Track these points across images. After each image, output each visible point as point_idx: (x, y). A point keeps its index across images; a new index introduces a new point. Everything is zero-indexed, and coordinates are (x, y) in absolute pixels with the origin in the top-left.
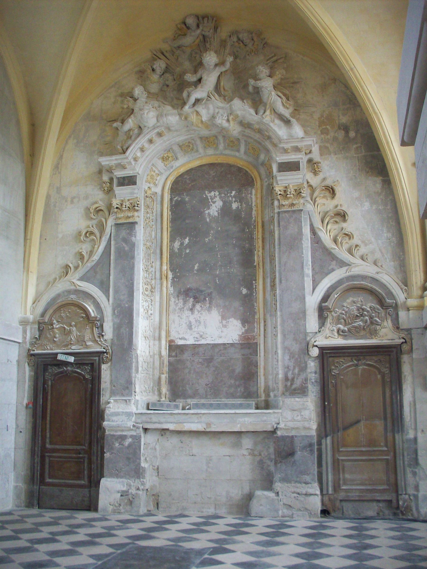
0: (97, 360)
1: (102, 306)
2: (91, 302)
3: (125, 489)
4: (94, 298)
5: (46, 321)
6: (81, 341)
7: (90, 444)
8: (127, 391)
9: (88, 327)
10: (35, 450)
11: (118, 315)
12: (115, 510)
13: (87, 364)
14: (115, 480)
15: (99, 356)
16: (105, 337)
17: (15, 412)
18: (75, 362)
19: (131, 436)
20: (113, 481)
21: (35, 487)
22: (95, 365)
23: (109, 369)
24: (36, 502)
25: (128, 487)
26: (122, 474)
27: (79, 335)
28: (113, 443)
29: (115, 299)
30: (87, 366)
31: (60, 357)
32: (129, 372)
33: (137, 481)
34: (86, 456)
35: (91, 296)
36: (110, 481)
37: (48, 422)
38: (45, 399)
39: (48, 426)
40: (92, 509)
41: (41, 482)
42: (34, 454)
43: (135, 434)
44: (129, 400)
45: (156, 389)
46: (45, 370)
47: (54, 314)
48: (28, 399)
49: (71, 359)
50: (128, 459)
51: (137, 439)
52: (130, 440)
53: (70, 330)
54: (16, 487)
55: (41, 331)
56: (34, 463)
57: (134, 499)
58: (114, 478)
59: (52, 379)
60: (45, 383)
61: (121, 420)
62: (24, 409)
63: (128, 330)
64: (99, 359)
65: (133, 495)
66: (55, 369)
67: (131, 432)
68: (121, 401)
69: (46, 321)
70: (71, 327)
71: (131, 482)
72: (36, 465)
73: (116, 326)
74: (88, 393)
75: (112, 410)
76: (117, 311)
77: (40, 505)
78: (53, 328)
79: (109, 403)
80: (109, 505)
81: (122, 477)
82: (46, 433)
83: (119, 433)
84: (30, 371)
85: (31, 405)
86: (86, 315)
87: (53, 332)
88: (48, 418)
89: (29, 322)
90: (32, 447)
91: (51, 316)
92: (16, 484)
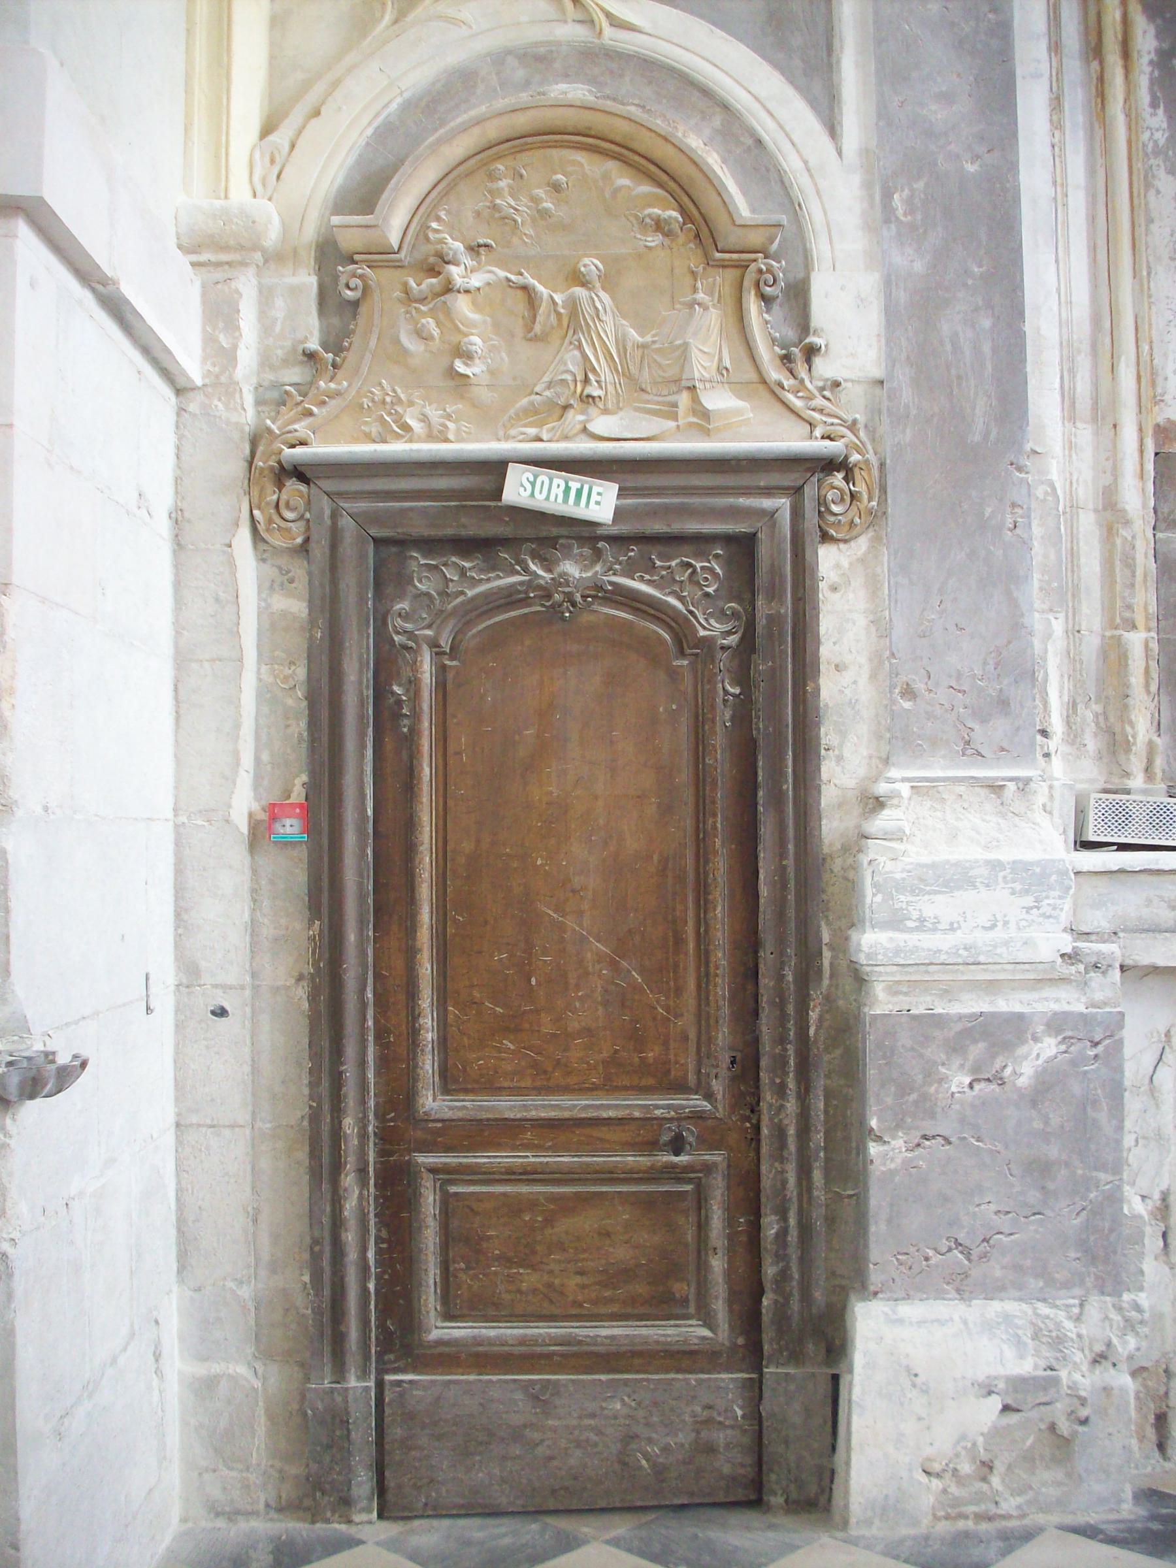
0: (785, 517)
1: (791, 163)
2: (707, 132)
3: (1026, 1367)
4: (725, 107)
5: (394, 239)
6: (673, 388)
7: (746, 1069)
8: (1000, 727)
9: (701, 296)
10: (337, 1134)
11: (913, 227)
12: (957, 1502)
13: (700, 543)
14: (950, 1310)
15: (798, 490)
16: (824, 368)
17: (170, 875)
18: (624, 529)
19: (1057, 1023)
20: (941, 1322)
21: (353, 1382)
22: (764, 551)
23: (858, 582)
24: (363, 1483)
25: (1047, 1353)
26: (998, 1273)
27: (643, 346)
28: (930, 1073)
29: (884, 117)
30: (701, 555)
31: (523, 489)
32: (1013, 603)
33: (1097, 1305)
34: (716, 1157)
35: (706, 92)
36: (921, 1323)
37: (424, 936)
38: (395, 783)
39: (426, 968)
40: (777, 1500)
41: (387, 1342)
42: (337, 1167)
43: (1080, 1008)
44: (1024, 785)
45: (1090, 716)
46: (387, 579)
47: (446, 193)
48: (256, 787)
49: (600, 502)
50: (1040, 1169)
51: (1096, 1037)
52: (1049, 1047)
53: (574, 306)
54: (205, 1388)
55: (340, 308)
56: (337, 1223)
57: (1084, 1422)
58: (940, 1295)
59: (445, 643)
60: (387, 662)
61: (984, 920)
62: (238, 855)
63: (987, 323)
64: (797, 513)
65: (1083, 1401)
66: (463, 572)
67: (1049, 992)
68: (961, 789)
69: (394, 239)
70: (579, 291)
71: (1055, 1314)
72: (350, 1237)
73: (902, 296)
74: (719, 741)
75: (915, 854)
76: (909, 201)
77: (390, 1496)
78: (448, 288)
79: (878, 804)
80: (924, 1478)
81: (993, 1291)
82: (413, 1015)
83: (971, 1005)
84: (268, 587)
85: (290, 827)
86: (683, 211)
87: (446, 316)
88: (425, 916)
89: (256, 247)
90: (314, 1117)
91: (426, 208)
92: (201, 1370)
